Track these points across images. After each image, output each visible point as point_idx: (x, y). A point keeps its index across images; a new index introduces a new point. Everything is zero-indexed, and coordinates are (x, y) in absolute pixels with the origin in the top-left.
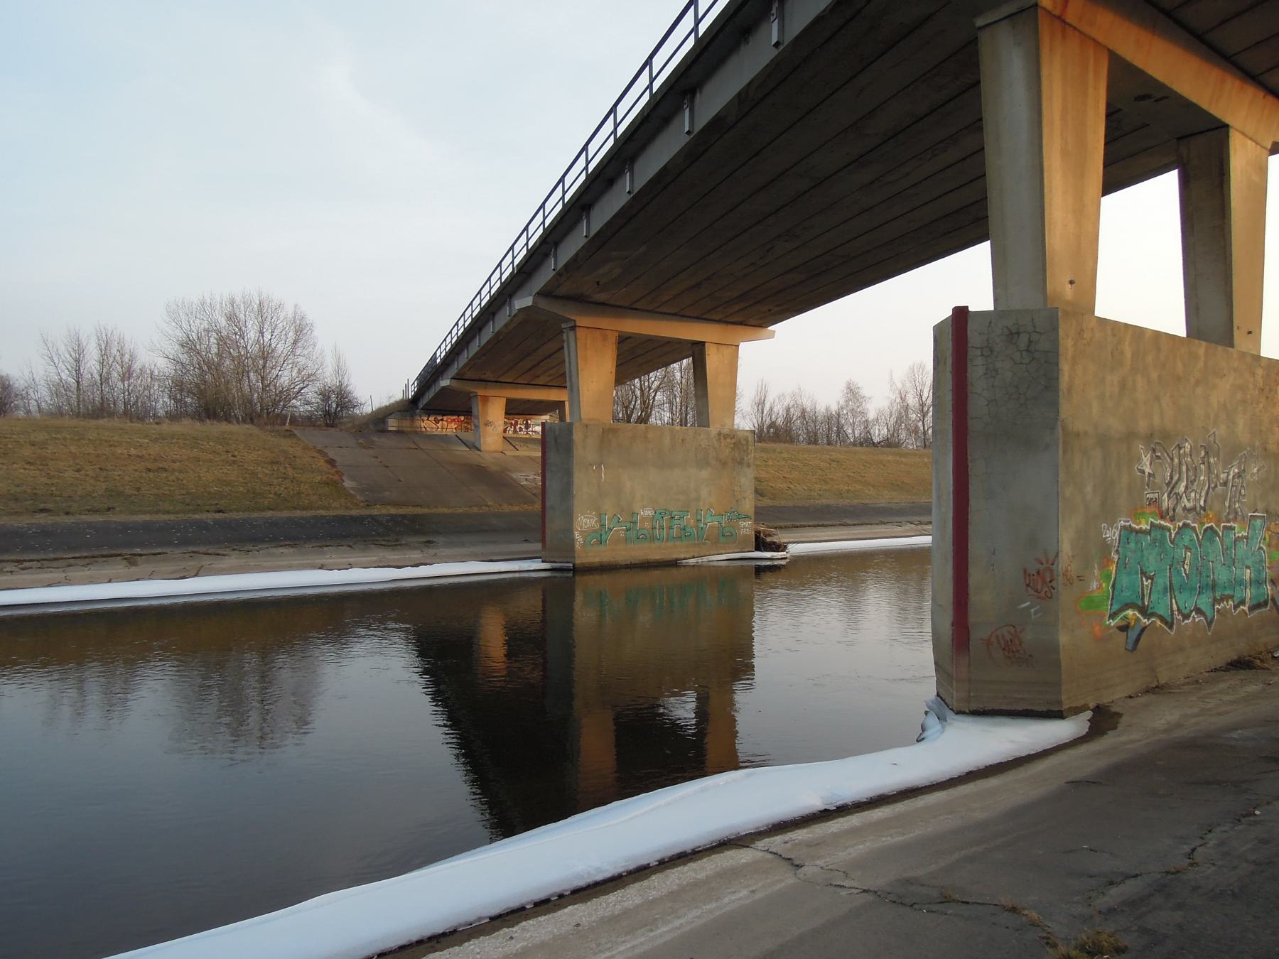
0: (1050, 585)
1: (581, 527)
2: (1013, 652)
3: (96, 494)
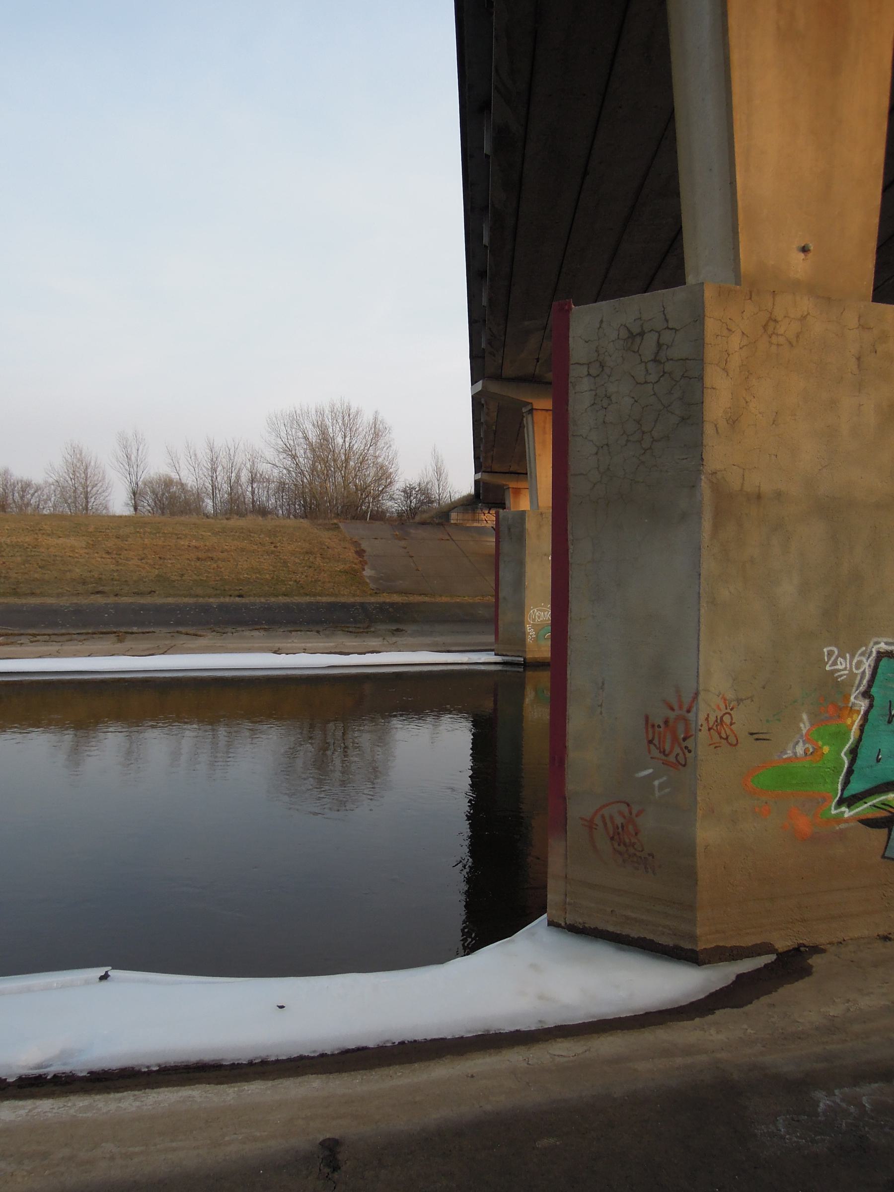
0: (684, 744)
1: (534, 620)
2: (625, 844)
3: (147, 579)
